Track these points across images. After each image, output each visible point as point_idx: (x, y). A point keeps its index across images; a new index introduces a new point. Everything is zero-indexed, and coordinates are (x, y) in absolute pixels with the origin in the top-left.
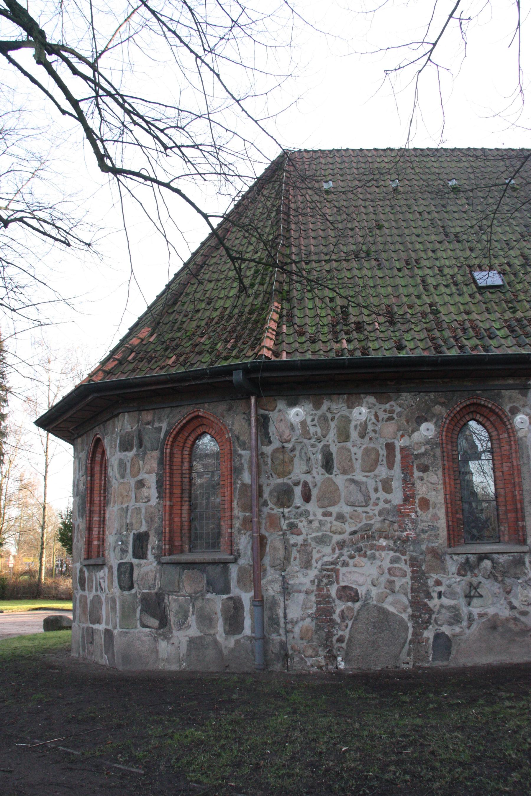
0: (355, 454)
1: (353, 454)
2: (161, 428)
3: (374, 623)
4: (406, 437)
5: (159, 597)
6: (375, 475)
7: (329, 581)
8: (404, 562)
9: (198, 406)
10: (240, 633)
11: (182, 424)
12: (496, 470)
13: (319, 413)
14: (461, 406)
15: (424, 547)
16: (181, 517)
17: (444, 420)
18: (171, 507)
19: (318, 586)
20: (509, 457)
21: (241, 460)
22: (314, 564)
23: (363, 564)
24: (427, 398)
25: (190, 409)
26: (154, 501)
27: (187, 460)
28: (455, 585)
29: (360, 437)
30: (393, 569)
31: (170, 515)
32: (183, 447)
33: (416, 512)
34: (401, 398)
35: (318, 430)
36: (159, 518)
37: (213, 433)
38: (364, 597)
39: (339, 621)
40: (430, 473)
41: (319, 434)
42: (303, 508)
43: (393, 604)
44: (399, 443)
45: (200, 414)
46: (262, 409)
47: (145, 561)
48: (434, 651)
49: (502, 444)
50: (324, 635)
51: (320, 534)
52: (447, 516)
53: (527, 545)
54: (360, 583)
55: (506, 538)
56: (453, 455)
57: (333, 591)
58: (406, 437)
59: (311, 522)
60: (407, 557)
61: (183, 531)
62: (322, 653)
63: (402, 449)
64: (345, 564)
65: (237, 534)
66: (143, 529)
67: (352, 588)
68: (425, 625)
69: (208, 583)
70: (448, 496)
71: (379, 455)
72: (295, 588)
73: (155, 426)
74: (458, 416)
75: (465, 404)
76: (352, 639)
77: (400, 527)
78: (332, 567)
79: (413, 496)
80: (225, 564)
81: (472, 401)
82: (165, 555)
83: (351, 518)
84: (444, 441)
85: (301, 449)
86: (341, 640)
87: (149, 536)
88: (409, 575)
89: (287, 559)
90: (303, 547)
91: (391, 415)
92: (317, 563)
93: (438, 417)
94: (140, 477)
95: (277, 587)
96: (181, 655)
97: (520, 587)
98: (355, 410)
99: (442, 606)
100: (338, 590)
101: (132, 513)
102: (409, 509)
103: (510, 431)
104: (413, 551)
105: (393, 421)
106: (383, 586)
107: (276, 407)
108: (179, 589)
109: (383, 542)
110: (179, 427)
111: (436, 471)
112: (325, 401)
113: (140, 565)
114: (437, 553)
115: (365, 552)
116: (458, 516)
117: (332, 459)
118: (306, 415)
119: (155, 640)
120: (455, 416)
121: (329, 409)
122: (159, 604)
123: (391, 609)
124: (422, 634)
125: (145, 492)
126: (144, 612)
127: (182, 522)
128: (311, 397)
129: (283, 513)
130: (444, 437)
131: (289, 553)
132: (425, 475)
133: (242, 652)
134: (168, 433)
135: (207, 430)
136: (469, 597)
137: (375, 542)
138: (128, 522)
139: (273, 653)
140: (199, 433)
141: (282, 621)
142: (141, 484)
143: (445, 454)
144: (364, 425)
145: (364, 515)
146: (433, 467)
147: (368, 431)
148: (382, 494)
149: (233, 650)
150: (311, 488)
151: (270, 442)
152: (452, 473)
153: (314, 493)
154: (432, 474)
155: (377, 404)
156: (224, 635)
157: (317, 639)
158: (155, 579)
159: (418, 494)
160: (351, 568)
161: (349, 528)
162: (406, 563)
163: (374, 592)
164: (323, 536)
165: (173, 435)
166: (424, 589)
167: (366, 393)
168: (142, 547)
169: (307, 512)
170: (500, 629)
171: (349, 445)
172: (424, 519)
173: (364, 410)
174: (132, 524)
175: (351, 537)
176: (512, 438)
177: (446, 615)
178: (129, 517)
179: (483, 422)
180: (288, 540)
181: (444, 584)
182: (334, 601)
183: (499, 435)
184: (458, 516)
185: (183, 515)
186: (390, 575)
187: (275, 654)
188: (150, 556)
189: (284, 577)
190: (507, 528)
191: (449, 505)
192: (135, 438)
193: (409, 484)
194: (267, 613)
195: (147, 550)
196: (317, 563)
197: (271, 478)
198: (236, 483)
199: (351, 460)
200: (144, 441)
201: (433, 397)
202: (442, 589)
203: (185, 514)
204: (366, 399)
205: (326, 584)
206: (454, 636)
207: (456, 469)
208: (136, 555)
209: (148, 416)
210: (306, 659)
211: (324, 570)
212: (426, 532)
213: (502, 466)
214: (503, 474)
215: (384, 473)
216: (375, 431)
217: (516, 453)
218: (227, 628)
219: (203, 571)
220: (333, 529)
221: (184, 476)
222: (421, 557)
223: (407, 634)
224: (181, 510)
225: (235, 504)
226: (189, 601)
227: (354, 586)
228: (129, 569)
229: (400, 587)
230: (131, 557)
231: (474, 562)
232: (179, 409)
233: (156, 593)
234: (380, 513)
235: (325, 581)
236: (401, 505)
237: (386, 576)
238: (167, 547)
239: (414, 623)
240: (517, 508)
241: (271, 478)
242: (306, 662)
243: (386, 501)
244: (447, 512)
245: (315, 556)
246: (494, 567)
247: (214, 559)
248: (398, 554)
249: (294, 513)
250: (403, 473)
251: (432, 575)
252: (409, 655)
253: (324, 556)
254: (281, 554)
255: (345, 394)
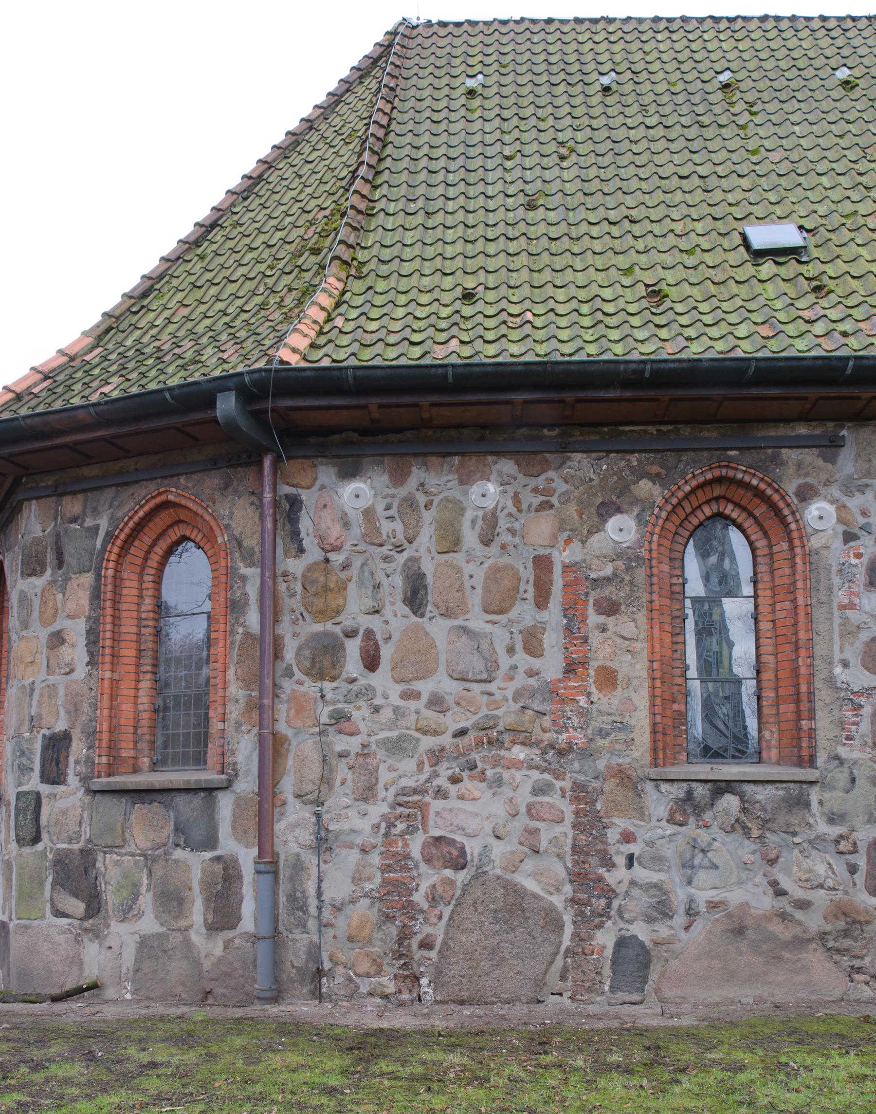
0: (471, 577)
1: (466, 577)
2: (97, 528)
3: (496, 911)
4: (576, 545)
5: (87, 855)
6: (509, 620)
7: (408, 827)
8: (559, 792)
9: (166, 482)
10: (233, 927)
11: (136, 519)
12: (760, 618)
13: (401, 492)
14: (694, 483)
15: (601, 765)
16: (135, 703)
17: (656, 510)
18: (115, 684)
19: (387, 835)
20: (792, 589)
21: (244, 586)
22: (382, 794)
23: (477, 794)
24: (623, 464)
25: (151, 487)
26: (81, 671)
27: (150, 592)
28: (662, 841)
29: (482, 542)
30: (538, 806)
31: (113, 697)
32: (143, 567)
33: (589, 695)
34: (569, 463)
35: (398, 526)
36: (90, 705)
37: (198, 540)
38: (476, 860)
39: (425, 905)
40: (623, 618)
41: (401, 537)
42: (362, 682)
43: (535, 875)
44: (561, 557)
45: (171, 497)
46: (288, 484)
47: (62, 788)
48: (614, 972)
49: (776, 565)
50: (395, 933)
51: (394, 734)
52: (653, 705)
53: (816, 768)
54: (469, 831)
55: (774, 753)
56: (672, 585)
57: (416, 846)
58: (576, 545)
59: (377, 709)
60: (567, 784)
61: (139, 731)
62: (391, 968)
63: (566, 568)
64: (441, 794)
65: (234, 733)
66: (61, 726)
67: (454, 841)
68: (597, 920)
69: (177, 829)
70: (656, 665)
71: (519, 580)
72: (342, 838)
73: (86, 525)
74: (685, 504)
75: (701, 479)
76: (451, 943)
77: (554, 723)
78: (415, 798)
79: (584, 664)
80: (210, 791)
81: (717, 473)
82: (99, 776)
83: (458, 704)
84: (655, 554)
85: (363, 565)
86: (426, 945)
87: (71, 740)
88: (569, 818)
89: (326, 781)
90: (361, 760)
91: (545, 498)
92: (387, 789)
93: (646, 505)
94: (56, 627)
95: (306, 836)
96: (124, 970)
97: (796, 851)
98: (474, 487)
99: (633, 883)
100: (425, 845)
101: (41, 695)
102: (574, 688)
103: (795, 535)
104: (579, 772)
105: (551, 512)
106: (515, 840)
107: (315, 480)
108: (124, 840)
109: (519, 753)
110: (131, 524)
111: (633, 613)
112: (414, 469)
113: (53, 796)
114: (629, 777)
115: (483, 772)
116: (676, 707)
117: (425, 587)
118: (375, 495)
119: (78, 941)
120: (679, 504)
121: (422, 484)
122: (86, 871)
123: (531, 885)
124: (591, 938)
125: (66, 653)
126: (58, 887)
127: (137, 713)
128: (386, 460)
129: (321, 690)
130: (654, 546)
131: (331, 770)
132: (611, 621)
133: (236, 965)
134: (110, 537)
135: (188, 534)
136: (687, 865)
137: (503, 753)
138: (33, 713)
139: (293, 966)
140: (174, 538)
141: (313, 903)
142: (58, 639)
143: (655, 580)
144: (491, 520)
145: (485, 698)
146: (628, 606)
147: (498, 530)
148: (522, 659)
149: (220, 960)
150: (381, 642)
151: (301, 550)
152: (668, 619)
153: (386, 653)
154: (626, 619)
155: (520, 476)
156: (204, 931)
157: (382, 940)
158: (80, 823)
159: (596, 659)
160: (453, 803)
161: (453, 722)
162: (563, 796)
163: (498, 850)
164: (400, 738)
165: (119, 542)
166: (600, 847)
167: (498, 454)
168: (58, 763)
169: (368, 692)
170: (750, 933)
171: (459, 558)
172: (604, 708)
173: (492, 488)
174: (40, 716)
175: (456, 740)
176: (798, 551)
177: (639, 902)
178: (34, 703)
179: (739, 520)
180: (330, 745)
181: (639, 840)
182: (416, 866)
183: (770, 546)
184: (676, 707)
185: (140, 701)
186: (532, 817)
187: (297, 968)
188: (72, 780)
189: (318, 816)
190: (776, 736)
191: (658, 683)
192: (49, 550)
193: (577, 638)
194: (284, 888)
195: (67, 766)
196: (387, 789)
197: (301, 621)
198: (233, 632)
199: (461, 589)
200: (66, 555)
201: (635, 463)
202: (634, 848)
203: (144, 698)
204: (498, 466)
205: (402, 834)
206: (656, 944)
207: (678, 613)
208: (46, 778)
209: (73, 506)
210: (358, 980)
211: (400, 805)
212: (608, 734)
213: (774, 611)
214: (774, 625)
215: (528, 617)
216: (512, 532)
217: (805, 580)
218: (210, 918)
219: (167, 806)
220: (422, 723)
221: (144, 623)
222: (595, 784)
223: (561, 936)
224: (137, 689)
225: (231, 673)
226: (141, 864)
227: (458, 838)
228: (33, 803)
229: (551, 842)
230: (38, 780)
231: (703, 797)
232: (131, 490)
233: (82, 851)
234: (517, 696)
235: (401, 826)
236: (559, 681)
237: (523, 820)
238: (104, 760)
239: (576, 915)
240: (798, 693)
241: (301, 621)
242: (358, 987)
243: (532, 673)
244: (653, 696)
245: (385, 777)
246: (744, 810)
247: (188, 782)
248: (546, 776)
249: (344, 690)
250: (565, 616)
251: (615, 820)
252: (563, 978)
253: (400, 777)
254: (314, 771)
255: (455, 454)
